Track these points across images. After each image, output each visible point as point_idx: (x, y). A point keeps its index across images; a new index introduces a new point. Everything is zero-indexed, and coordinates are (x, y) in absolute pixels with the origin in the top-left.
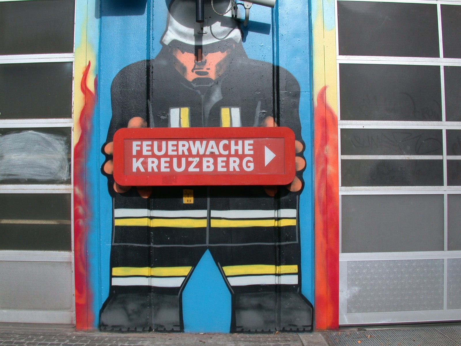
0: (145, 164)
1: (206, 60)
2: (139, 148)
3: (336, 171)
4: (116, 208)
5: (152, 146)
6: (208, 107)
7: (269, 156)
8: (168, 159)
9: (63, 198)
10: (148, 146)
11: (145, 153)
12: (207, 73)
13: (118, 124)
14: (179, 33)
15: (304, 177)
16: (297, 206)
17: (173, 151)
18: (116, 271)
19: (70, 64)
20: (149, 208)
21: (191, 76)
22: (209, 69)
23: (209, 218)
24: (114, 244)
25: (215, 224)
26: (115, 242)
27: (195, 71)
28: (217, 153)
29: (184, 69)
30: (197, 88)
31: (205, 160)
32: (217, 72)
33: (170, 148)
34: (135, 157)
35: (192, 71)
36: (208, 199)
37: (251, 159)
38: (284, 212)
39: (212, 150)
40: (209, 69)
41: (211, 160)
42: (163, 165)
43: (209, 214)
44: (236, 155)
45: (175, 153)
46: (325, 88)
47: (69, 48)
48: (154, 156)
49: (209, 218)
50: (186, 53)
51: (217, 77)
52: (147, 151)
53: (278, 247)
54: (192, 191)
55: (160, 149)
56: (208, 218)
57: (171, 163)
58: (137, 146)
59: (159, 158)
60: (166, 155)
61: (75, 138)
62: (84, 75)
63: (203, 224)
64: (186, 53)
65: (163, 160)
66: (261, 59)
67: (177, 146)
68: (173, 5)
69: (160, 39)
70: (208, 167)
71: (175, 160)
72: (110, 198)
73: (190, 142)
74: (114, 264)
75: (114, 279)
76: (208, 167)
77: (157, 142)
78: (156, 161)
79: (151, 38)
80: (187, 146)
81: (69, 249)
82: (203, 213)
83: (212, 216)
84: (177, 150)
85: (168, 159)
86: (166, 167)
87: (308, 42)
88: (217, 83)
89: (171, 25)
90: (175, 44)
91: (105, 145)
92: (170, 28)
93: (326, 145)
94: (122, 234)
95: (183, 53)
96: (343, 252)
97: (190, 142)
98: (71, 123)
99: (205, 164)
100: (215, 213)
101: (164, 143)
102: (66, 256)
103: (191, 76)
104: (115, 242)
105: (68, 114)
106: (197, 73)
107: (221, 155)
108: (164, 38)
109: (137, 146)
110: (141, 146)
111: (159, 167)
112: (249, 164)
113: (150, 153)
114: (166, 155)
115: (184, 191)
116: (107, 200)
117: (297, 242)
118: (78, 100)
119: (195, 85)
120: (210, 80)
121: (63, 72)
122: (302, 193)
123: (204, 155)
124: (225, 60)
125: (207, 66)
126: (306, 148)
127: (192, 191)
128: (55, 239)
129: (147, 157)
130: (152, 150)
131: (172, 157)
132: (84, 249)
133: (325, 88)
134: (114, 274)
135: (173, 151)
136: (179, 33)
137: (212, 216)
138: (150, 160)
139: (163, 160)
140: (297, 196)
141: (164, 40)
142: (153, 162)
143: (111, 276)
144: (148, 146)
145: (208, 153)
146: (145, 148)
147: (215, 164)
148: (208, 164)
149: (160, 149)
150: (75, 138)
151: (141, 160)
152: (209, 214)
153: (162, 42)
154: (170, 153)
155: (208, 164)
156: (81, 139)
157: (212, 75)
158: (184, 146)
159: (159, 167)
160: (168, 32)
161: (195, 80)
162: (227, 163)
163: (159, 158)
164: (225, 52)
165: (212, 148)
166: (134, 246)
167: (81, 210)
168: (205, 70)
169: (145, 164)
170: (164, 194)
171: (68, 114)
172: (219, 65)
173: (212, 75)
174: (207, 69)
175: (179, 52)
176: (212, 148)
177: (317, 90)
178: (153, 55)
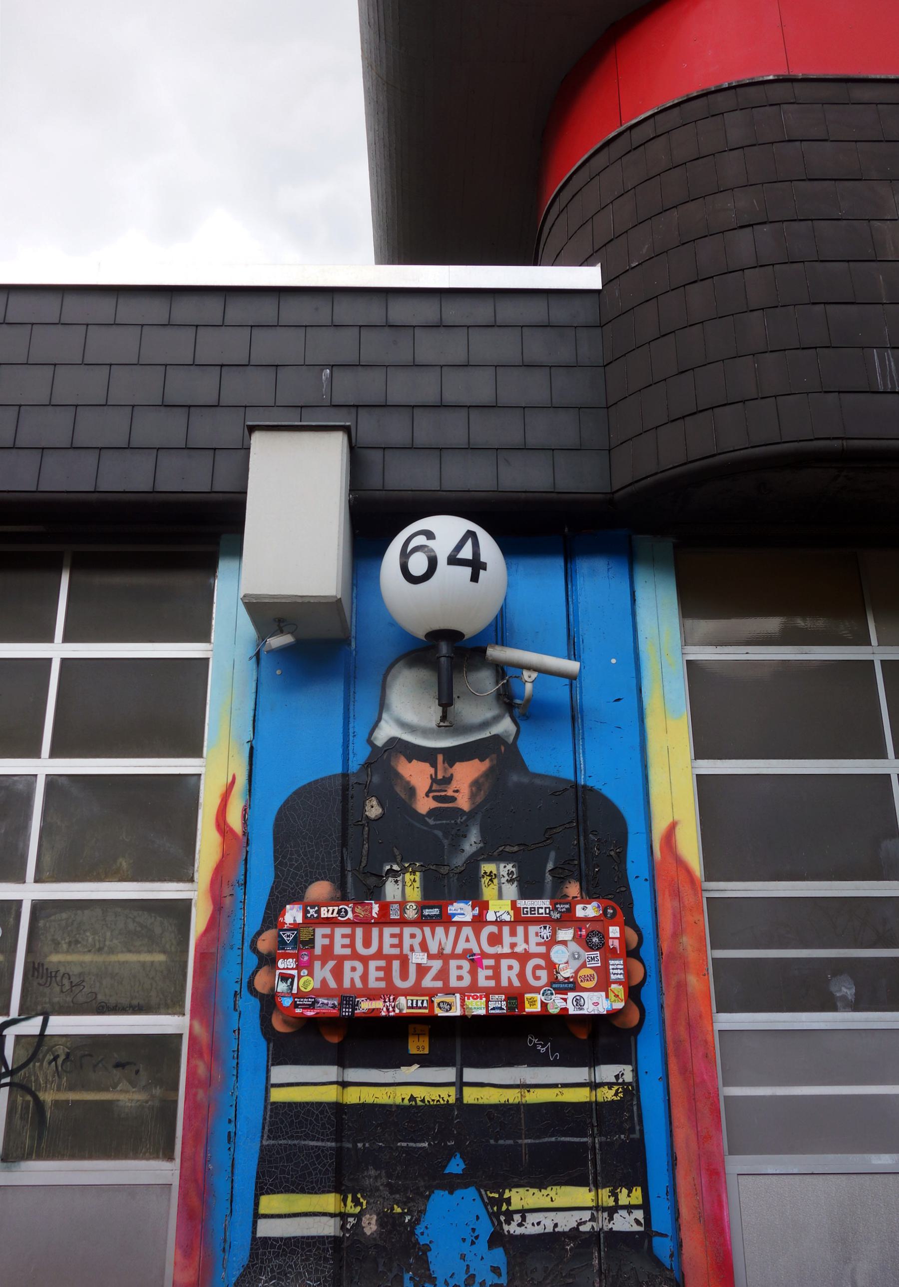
0: (337, 972)
1: (452, 775)
2: (326, 941)
3: (700, 984)
4: (273, 1065)
5: (352, 937)
6: (459, 861)
7: (367, 1145)
8: (382, 963)
9: (166, 1045)
10: (344, 936)
11: (338, 950)
12: (453, 799)
13: (285, 891)
14: (403, 725)
15: (643, 999)
16: (633, 1059)
17: (392, 946)
18: (270, 1203)
19: (196, 777)
20: (342, 1064)
21: (424, 805)
22: (457, 791)
23: (460, 1084)
24: (265, 1143)
25: (471, 1096)
26: (269, 1138)
27: (431, 795)
28: (476, 950)
29: (412, 791)
30: (435, 827)
31: (453, 963)
32: (473, 796)
33: (388, 941)
34: (318, 958)
35: (427, 795)
36: (458, 1043)
37: (542, 962)
38: (607, 1072)
39: (467, 946)
40: (457, 791)
41: (466, 965)
42: (373, 974)
43: (460, 1075)
44: (513, 955)
45: (396, 951)
46: (672, 827)
47: (194, 749)
48: (355, 956)
49: (460, 1084)
50: (414, 761)
51: (473, 806)
52: (343, 946)
53: (600, 1146)
54: (426, 1028)
55: (367, 943)
56: (458, 1084)
57: (388, 970)
58: (324, 936)
59: (365, 960)
60: (379, 955)
61: (198, 922)
62: (222, 800)
63: (448, 1095)
64: (414, 761)
65: (373, 964)
66: (552, 772)
67: (400, 936)
68: (391, 674)
69: (366, 736)
70: (460, 978)
71: (396, 964)
72: (263, 1043)
73: (425, 928)
74: (263, 1188)
75: (261, 1223)
76: (460, 978)
77: (361, 929)
78: (359, 965)
79: (351, 735)
80: (419, 938)
81: (170, 1157)
82: (448, 1074)
83: (465, 1079)
84: (400, 945)
85: (382, 963)
86: (378, 979)
87: (638, 740)
88: (471, 814)
89: (388, 709)
90: (396, 746)
91: (259, 934)
92: (385, 716)
93: (345, 788)
94: (285, 1119)
95: (410, 762)
96: (730, 1154)
97: (425, 928)
98: (195, 892)
99: (453, 973)
100: (470, 1075)
101: (375, 931)
102: (163, 1172)
103: (424, 805)
104: (269, 1138)
105: (182, 871)
106: (435, 798)
107: (484, 955)
108: (375, 734)
109: (324, 936)
110: (331, 937)
111: (365, 977)
112: (539, 973)
113: (348, 951)
114: (379, 955)
115: (411, 1028)
116: (255, 1047)
117: (637, 1136)
118: (208, 847)
119: (431, 822)
120: (459, 811)
121: (184, 789)
122: (643, 1031)
123: (454, 956)
124: (487, 774)
125: (454, 785)
126: (645, 940)
127: (426, 1028)
128: (145, 1135)
129: (341, 959)
130: (352, 945)
131: (389, 959)
132: (202, 1155)
133: (672, 827)
134: (262, 1210)
135: (392, 946)
136: (403, 725)
137: (465, 1079)
138: (348, 965)
139: (373, 964)
140: (632, 1038)
141: (375, 738)
142: (354, 969)
143: (257, 1216)
144: (344, 936)
145: (459, 950)
146: (339, 941)
147: (473, 973)
148: (460, 972)
149: (367, 943)
150: (198, 922)
151: (331, 964)
152: (460, 1075)
153: (370, 742)
154: (387, 950)
155: (460, 972)
156: (213, 923)
157: (464, 802)
158: (413, 936)
159: (365, 977)
160: (383, 724)
161: (432, 812)
162: (496, 969)
163: (365, 960)
164: (487, 760)
165: (467, 940)
166: (304, 1147)
167: (202, 1070)
168: (450, 793)
169: (337, 972)
170: (370, 1038)
171: (182, 871)
172: (476, 784)
173: (464, 802)
174: (454, 791)
175: (403, 760)
176: (467, 940)
177: (659, 827)
178: (354, 766)
